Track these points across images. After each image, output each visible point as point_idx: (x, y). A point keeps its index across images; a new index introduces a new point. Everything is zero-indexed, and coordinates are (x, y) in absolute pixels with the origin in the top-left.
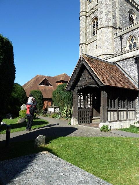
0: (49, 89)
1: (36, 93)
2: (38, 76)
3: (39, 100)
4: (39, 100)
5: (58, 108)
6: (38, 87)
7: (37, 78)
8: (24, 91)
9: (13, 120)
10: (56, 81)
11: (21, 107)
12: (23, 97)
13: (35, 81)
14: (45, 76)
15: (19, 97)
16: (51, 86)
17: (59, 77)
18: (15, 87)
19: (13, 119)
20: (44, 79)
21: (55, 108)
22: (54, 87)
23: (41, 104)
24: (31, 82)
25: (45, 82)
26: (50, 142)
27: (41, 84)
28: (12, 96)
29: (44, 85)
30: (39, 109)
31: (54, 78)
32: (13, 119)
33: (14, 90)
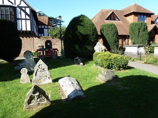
0: (118, 25)
1: (109, 27)
2: (103, 10)
3: (114, 37)
4: (114, 37)
5: (143, 46)
6: (104, 22)
7: (102, 13)
8: (93, 25)
9: (83, 66)
10: (125, 14)
11: (96, 48)
12: (94, 33)
13: (100, 16)
14: (111, 10)
15: (89, 33)
16: (119, 20)
17: (130, 8)
18: (82, 20)
19: (84, 65)
20: (111, 12)
21: (139, 47)
22: (123, 22)
23: (116, 42)
24: (96, 17)
25: (113, 16)
26: (33, 17)
27: (107, 19)
28: (79, 32)
29: (111, 19)
30: (113, 49)
31: (122, 12)
32: (84, 65)
33: (81, 23)
